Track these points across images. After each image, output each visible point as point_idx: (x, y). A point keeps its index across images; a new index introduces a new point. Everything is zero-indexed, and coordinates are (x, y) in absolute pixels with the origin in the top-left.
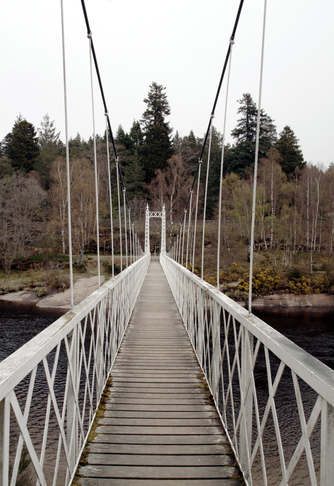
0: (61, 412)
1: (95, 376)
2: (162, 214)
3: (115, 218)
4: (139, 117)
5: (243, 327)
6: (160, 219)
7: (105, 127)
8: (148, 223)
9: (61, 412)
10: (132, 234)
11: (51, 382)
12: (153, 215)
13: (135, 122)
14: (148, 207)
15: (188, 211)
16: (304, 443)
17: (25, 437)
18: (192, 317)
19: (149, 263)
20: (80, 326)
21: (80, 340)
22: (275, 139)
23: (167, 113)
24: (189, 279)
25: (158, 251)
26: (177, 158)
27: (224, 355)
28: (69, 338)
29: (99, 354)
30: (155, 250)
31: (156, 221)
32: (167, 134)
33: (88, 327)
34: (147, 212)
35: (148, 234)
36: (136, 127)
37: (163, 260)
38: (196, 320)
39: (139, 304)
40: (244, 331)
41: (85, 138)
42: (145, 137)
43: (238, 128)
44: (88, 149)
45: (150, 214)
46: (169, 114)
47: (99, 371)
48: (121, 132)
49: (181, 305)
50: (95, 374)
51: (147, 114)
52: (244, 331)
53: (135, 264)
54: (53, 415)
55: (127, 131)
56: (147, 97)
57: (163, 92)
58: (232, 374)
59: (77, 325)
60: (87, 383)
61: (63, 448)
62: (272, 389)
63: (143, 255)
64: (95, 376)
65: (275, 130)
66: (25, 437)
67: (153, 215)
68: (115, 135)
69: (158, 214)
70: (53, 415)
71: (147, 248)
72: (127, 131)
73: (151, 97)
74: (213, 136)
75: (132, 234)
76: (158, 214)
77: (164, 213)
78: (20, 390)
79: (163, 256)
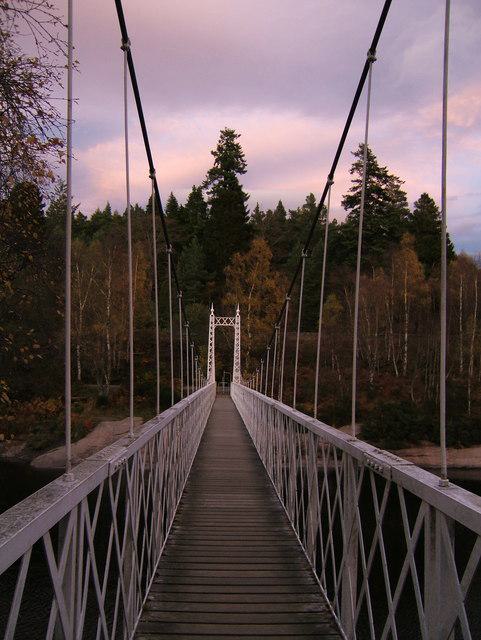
1: (121, 600)
2: (234, 322)
3: (164, 325)
4: (202, 176)
5: (428, 508)
6: (232, 330)
7: (150, 192)
10: (184, 345)
12: (222, 321)
14: (212, 310)
18: (293, 484)
19: (213, 398)
20: (85, 508)
22: (406, 212)
23: (242, 171)
24: (286, 418)
25: (229, 379)
26: (259, 243)
30: (224, 377)
31: (224, 335)
32: (242, 203)
33: (105, 506)
34: (212, 319)
36: (196, 195)
37: (238, 393)
38: (303, 492)
39: (196, 473)
40: (433, 520)
41: (119, 208)
42: (210, 207)
43: (352, 194)
45: (216, 321)
46: (244, 172)
47: (127, 592)
48: (173, 201)
49: (271, 461)
50: (121, 593)
51: (213, 173)
52: (433, 520)
53: (189, 398)
55: (183, 200)
56: (215, 149)
57: (236, 141)
58: (388, 623)
59: (79, 505)
60: (102, 620)
62: (379, 516)
63: (203, 385)
64: (121, 600)
65: (405, 199)
67: (222, 321)
68: (164, 203)
71: (212, 375)
72: (183, 200)
73: (220, 149)
74: (315, 211)
75: (184, 345)
76: (228, 321)
77: (238, 319)
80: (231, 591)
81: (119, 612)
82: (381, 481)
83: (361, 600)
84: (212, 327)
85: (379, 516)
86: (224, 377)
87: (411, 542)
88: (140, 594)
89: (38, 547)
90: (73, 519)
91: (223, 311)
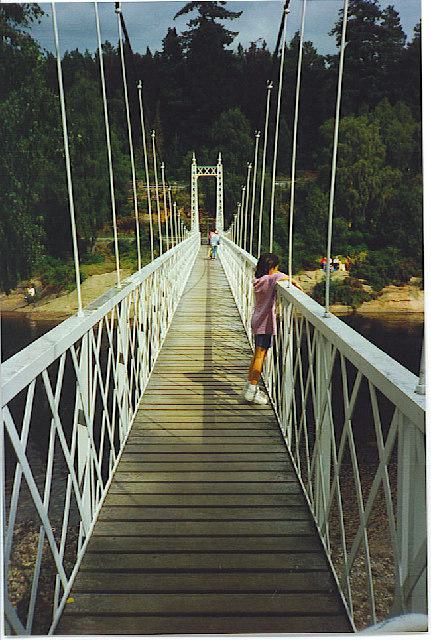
0: (70, 449)
8: (196, 190)
9: (70, 449)
11: (54, 402)
13: (225, 14)
14: (194, 160)
15: (253, 165)
16: (383, 473)
17: (23, 467)
20: (91, 334)
21: (93, 353)
27: (344, 454)
28: (78, 345)
29: (120, 372)
30: (207, 229)
31: (207, 185)
33: (105, 335)
34: (194, 168)
35: (197, 203)
44: (171, 173)
54: (57, 535)
61: (73, 496)
62: (349, 407)
66: (23, 467)
67: (204, 171)
69: (210, 171)
70: (57, 535)
76: (210, 171)
77: (220, 168)
78: (16, 406)
79: (220, 234)
80: (266, 455)
81: (411, 528)
82: (352, 370)
83: (333, 492)
84: (195, 177)
85: (349, 407)
86: (207, 229)
87: (384, 451)
88: (131, 410)
89: (68, 352)
90: (85, 337)
91: (205, 160)
